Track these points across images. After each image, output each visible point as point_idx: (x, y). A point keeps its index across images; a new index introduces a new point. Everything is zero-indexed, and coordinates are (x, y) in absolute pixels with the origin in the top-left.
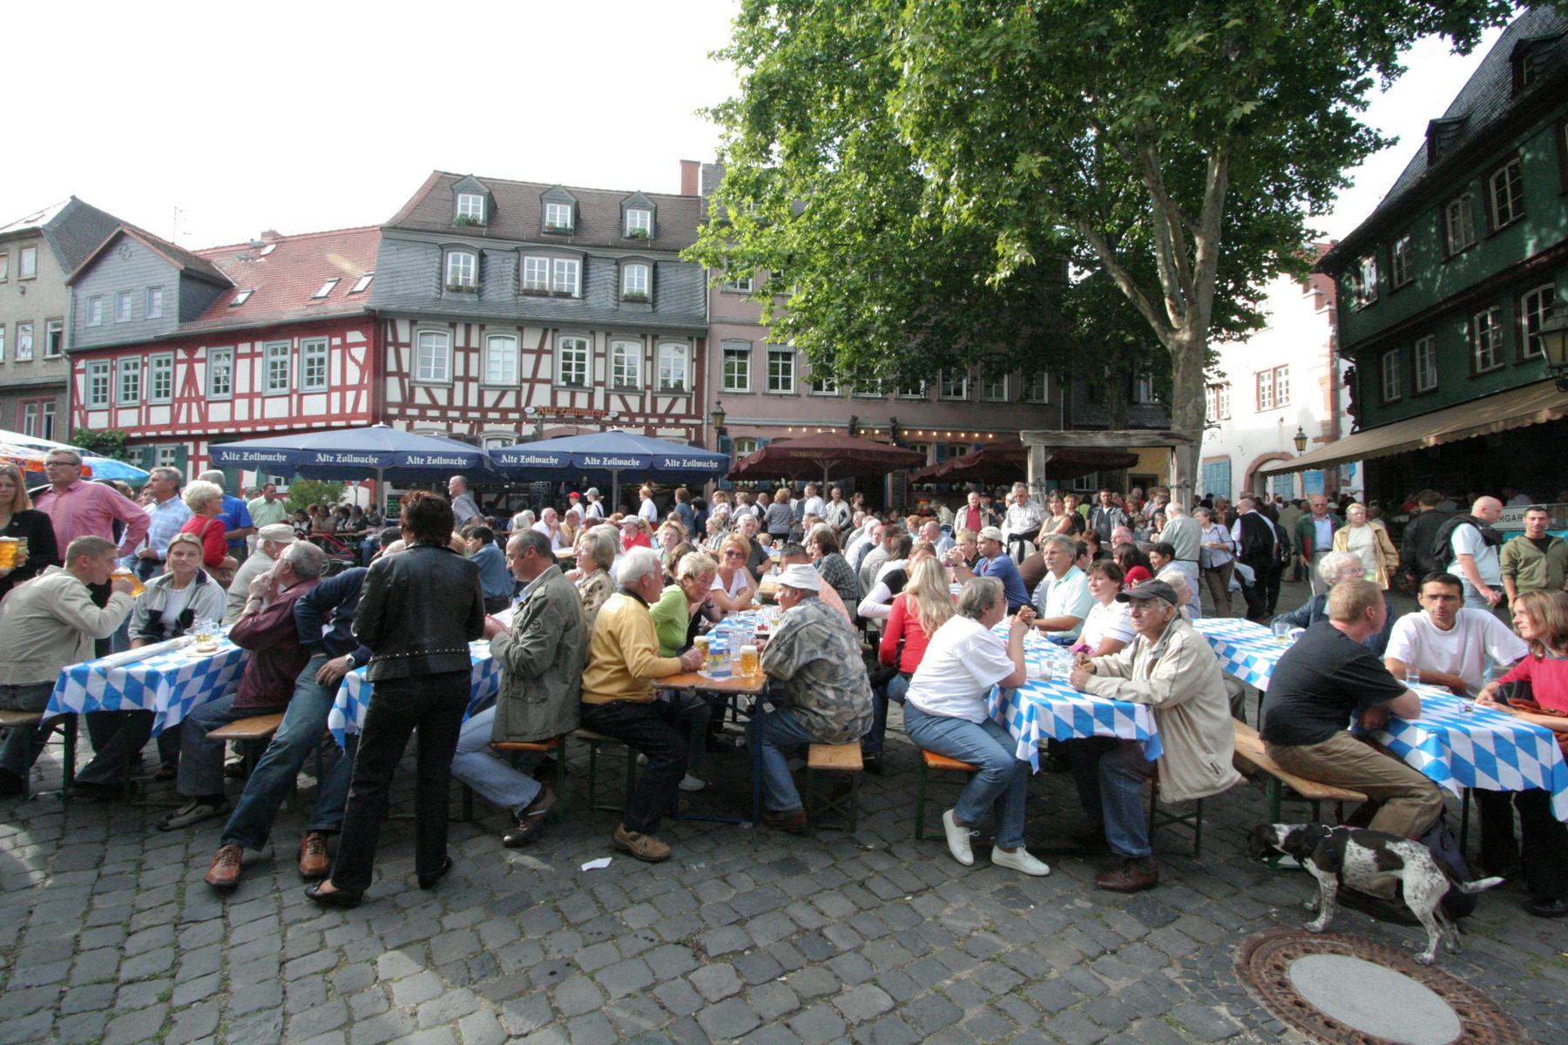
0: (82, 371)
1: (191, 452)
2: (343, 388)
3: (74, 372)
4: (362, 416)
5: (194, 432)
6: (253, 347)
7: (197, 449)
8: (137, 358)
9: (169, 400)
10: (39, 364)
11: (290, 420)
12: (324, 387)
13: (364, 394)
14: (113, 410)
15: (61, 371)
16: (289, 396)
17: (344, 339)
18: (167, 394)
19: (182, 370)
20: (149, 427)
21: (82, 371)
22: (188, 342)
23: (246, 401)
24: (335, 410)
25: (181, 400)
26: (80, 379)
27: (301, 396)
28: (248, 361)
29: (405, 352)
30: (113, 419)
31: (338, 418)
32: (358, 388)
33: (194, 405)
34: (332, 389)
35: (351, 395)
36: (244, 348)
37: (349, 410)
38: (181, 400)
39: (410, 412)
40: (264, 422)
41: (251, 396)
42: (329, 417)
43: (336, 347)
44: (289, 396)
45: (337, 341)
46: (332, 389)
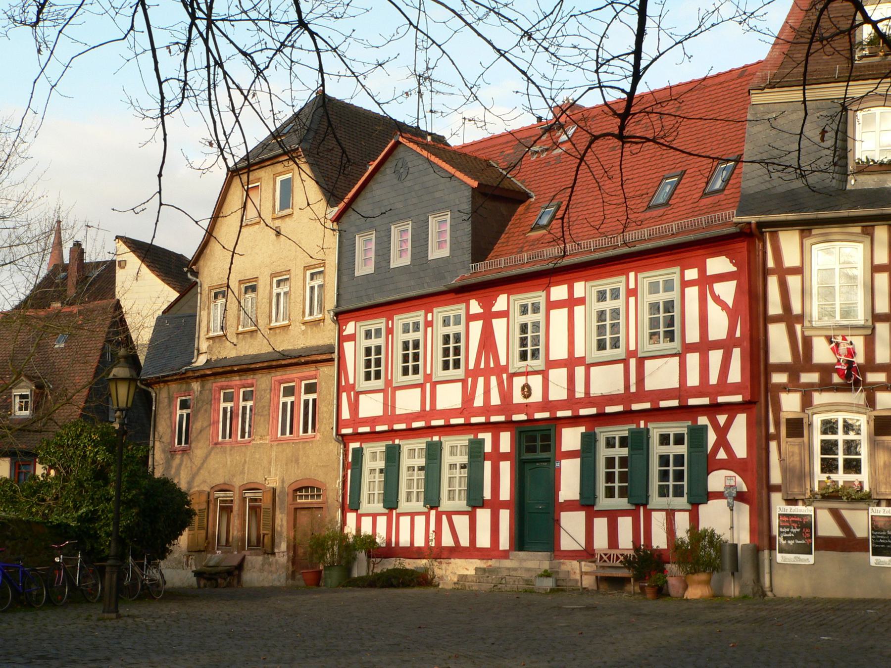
0: (352, 338)
1: (488, 448)
2: (704, 346)
3: (342, 339)
4: (734, 389)
5: (494, 419)
6: (571, 291)
7: (496, 442)
8: (418, 316)
9: (460, 373)
10: (297, 329)
11: (626, 397)
12: (676, 345)
13: (737, 352)
14: (389, 392)
15: (327, 335)
16: (422, 386)
17: (702, 270)
18: (457, 364)
19: (476, 327)
20: (435, 413)
21: (352, 338)
22: (485, 288)
23: (563, 372)
24: (693, 380)
25: (474, 374)
26: (348, 347)
27: (641, 362)
28: (564, 311)
29: (793, 282)
30: (389, 404)
31: (697, 392)
32: (725, 346)
33: (493, 380)
34: (689, 348)
35: (715, 357)
36: (559, 292)
37: (713, 379)
38: (474, 374)
39: (808, 378)
40: (589, 401)
41: (571, 363)
42: (683, 391)
43: (691, 283)
44: (625, 362)
45: (692, 274)
46: (689, 348)
